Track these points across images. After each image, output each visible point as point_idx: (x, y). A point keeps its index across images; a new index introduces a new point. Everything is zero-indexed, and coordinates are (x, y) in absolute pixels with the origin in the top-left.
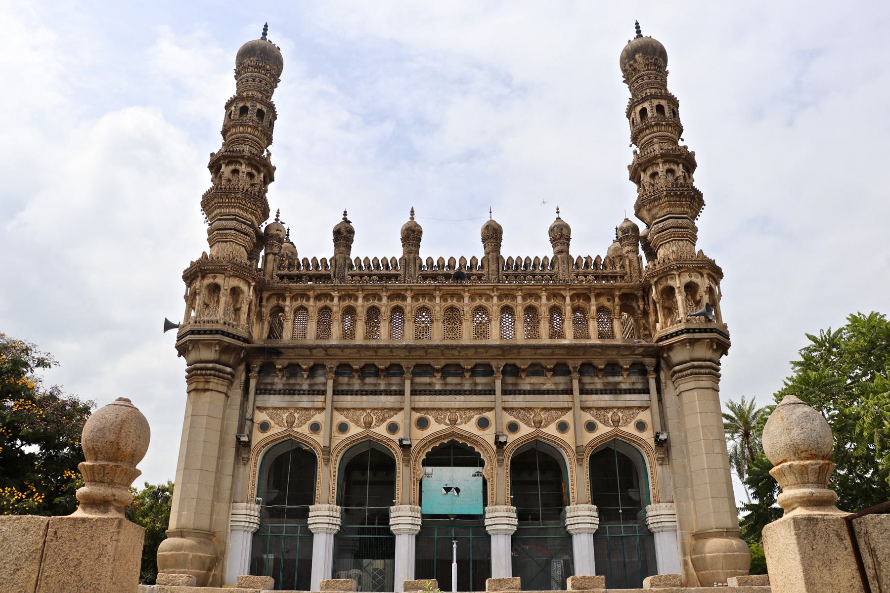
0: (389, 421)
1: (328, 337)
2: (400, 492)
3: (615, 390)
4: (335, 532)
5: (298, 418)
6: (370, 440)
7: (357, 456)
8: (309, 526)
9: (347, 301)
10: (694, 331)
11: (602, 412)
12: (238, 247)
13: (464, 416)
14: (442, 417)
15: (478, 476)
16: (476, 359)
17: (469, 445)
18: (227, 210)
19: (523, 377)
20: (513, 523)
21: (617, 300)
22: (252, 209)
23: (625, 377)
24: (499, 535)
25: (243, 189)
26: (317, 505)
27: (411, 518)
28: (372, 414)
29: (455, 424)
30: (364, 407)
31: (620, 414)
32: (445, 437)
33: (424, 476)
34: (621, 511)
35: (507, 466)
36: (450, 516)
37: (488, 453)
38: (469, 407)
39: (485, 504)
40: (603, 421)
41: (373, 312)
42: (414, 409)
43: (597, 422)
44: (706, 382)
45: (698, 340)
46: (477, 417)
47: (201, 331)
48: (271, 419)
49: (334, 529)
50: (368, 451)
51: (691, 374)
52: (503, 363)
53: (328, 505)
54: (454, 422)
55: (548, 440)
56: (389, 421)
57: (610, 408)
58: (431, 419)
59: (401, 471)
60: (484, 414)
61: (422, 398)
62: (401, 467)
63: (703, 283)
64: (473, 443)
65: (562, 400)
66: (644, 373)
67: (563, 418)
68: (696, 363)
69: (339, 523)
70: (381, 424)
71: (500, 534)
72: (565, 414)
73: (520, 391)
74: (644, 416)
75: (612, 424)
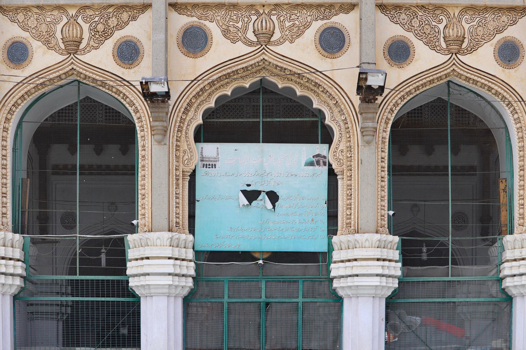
2: (147, 201)
6: (79, 82)
13: (288, 24)
14: (240, 25)
15: (318, 163)
17: (299, 92)
20: (393, 272)
27: (172, 261)
28: (80, 20)
29: (269, 42)
33: (200, 164)
35: (383, 142)
36: (257, 255)
37: (341, 112)
39: (332, 230)
46: (317, 25)
49: (11, 285)
50: (77, 102)
55: (475, 82)
56: (118, 35)
59: (148, 153)
60: (335, 19)
62: (148, 145)
64: (308, 88)
67: (511, 32)
69: (20, 271)
70: (101, 43)
71: (363, 296)
72: (514, 23)
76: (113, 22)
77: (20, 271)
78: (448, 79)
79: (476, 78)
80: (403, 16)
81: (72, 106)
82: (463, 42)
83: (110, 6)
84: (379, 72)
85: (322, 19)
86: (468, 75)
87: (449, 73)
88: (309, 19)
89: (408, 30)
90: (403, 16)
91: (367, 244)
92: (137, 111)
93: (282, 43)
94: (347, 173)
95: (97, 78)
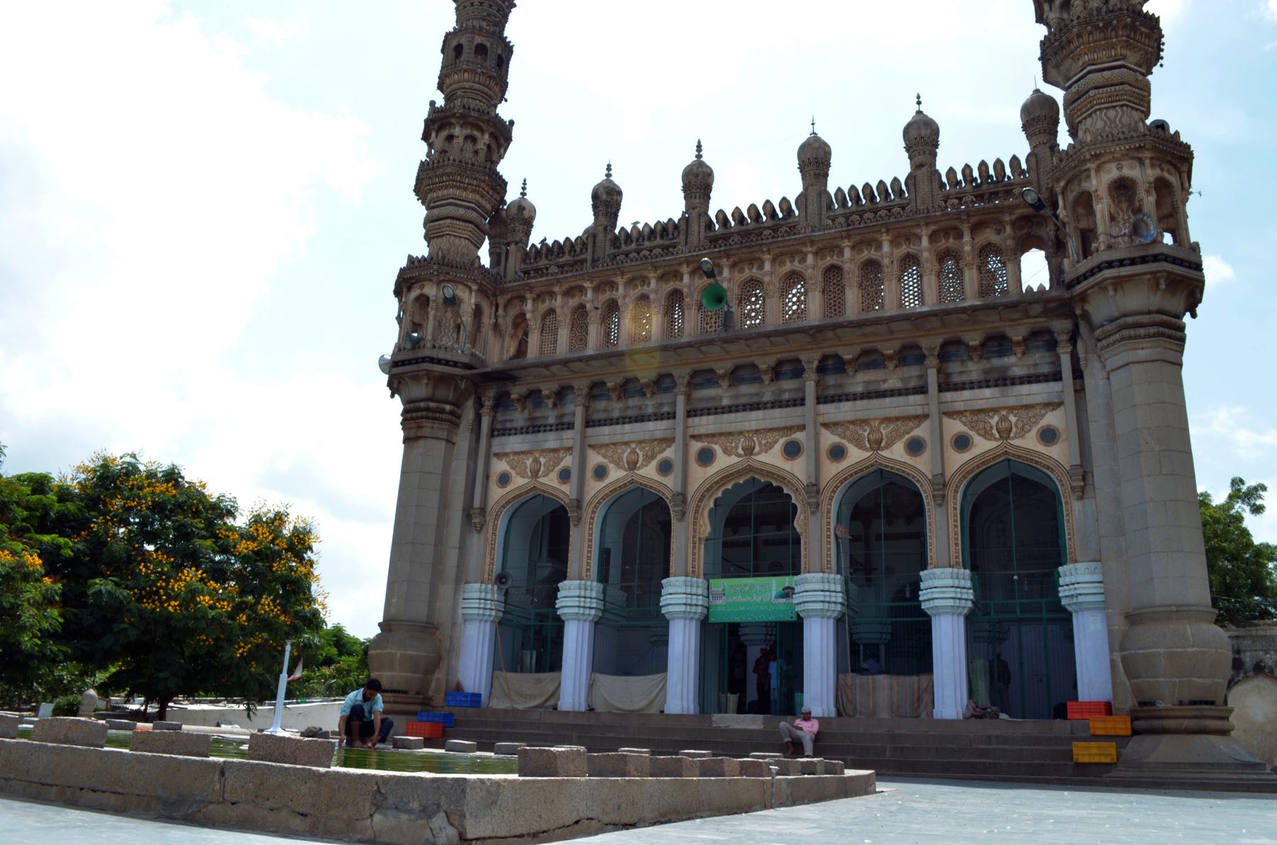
0: (660, 457)
1: (841, 313)
3: (1003, 380)
4: (965, 611)
5: (544, 465)
7: (984, 491)
8: (923, 604)
9: (866, 252)
10: (1121, 263)
11: (982, 417)
12: (457, 241)
13: (764, 442)
14: (733, 445)
16: (777, 353)
18: (440, 193)
19: (851, 374)
21: (1008, 229)
22: (473, 185)
23: (1019, 355)
24: (1085, 612)
25: (454, 160)
26: (672, 579)
28: (637, 450)
30: (626, 440)
31: (1012, 419)
32: (739, 473)
34: (1016, 577)
38: (770, 427)
40: (982, 432)
41: (871, 267)
42: (694, 437)
43: (973, 434)
44: (1150, 350)
45: (1130, 278)
46: (782, 441)
47: (1124, 260)
48: (513, 468)
51: (1122, 339)
52: (817, 355)
53: (821, 575)
54: (749, 451)
56: (660, 457)
57: (995, 410)
58: (717, 449)
61: (705, 419)
63: (1142, 174)
65: (913, 404)
66: (1052, 345)
68: (1130, 320)
69: (840, 600)
72: (918, 426)
73: (847, 395)
74: (1051, 418)
75: (997, 436)
77: (840, 600)
81: (1004, 479)
83: (656, 440)
85: (787, 436)
91: (814, 580)
92: (922, 485)
94: (804, 534)
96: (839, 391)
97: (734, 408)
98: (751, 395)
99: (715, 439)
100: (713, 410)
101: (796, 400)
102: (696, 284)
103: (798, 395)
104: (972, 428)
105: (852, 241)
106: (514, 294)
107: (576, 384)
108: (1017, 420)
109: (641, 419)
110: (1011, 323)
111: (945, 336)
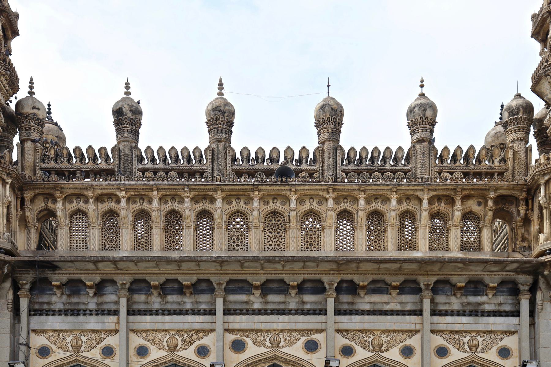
0: (197, 343)
11: (458, 335)
13: (288, 339)
14: (262, 339)
21: (490, 203)
23: (490, 296)
28: (177, 336)
29: (278, 347)
30: (167, 328)
31: (480, 339)
38: (294, 328)
40: (457, 346)
46: (303, 339)
56: (197, 343)
57: (468, 332)
58: (249, 341)
61: (238, 318)
65: (410, 322)
67: (409, 342)
72: (411, 338)
73: (357, 311)
74: (510, 342)
75: (468, 350)
76: (195, 337)
78: (374, 363)
79: (389, 363)
80: (350, 335)
82: (382, 346)
83: (193, 330)
84: (336, 360)
85: (307, 336)
86: (385, 362)
87: (374, 361)
88: (299, 336)
89: (352, 341)
90: (350, 335)
93: (285, 347)
95: (186, 363)
96: (351, 307)
97: (263, 312)
98: (315, 303)
99: (247, 334)
100: (244, 312)
101: (316, 310)
102: (99, 208)
103: (417, 307)
104: (450, 343)
105: (367, 194)
106: (41, 191)
107: (119, 279)
108: (483, 340)
109: (180, 312)
110: (489, 273)
111: (439, 277)
